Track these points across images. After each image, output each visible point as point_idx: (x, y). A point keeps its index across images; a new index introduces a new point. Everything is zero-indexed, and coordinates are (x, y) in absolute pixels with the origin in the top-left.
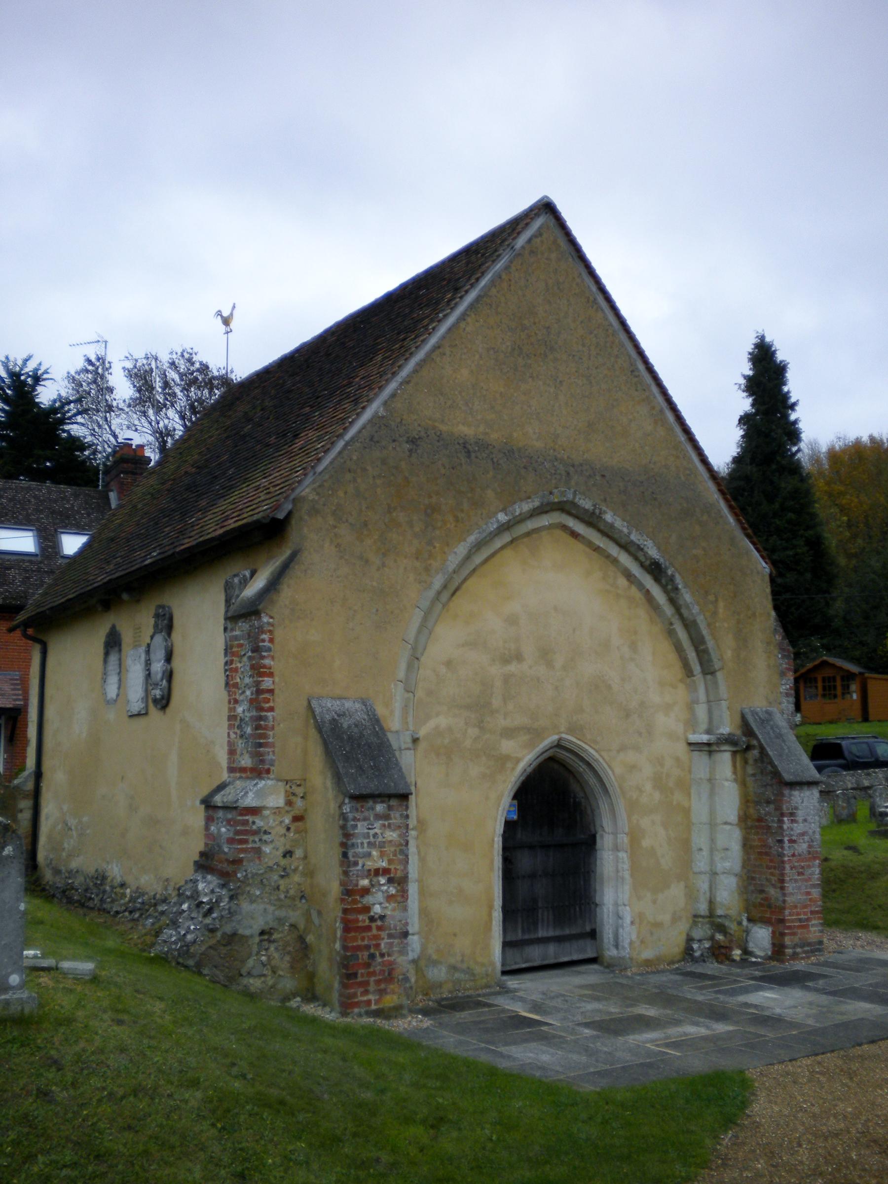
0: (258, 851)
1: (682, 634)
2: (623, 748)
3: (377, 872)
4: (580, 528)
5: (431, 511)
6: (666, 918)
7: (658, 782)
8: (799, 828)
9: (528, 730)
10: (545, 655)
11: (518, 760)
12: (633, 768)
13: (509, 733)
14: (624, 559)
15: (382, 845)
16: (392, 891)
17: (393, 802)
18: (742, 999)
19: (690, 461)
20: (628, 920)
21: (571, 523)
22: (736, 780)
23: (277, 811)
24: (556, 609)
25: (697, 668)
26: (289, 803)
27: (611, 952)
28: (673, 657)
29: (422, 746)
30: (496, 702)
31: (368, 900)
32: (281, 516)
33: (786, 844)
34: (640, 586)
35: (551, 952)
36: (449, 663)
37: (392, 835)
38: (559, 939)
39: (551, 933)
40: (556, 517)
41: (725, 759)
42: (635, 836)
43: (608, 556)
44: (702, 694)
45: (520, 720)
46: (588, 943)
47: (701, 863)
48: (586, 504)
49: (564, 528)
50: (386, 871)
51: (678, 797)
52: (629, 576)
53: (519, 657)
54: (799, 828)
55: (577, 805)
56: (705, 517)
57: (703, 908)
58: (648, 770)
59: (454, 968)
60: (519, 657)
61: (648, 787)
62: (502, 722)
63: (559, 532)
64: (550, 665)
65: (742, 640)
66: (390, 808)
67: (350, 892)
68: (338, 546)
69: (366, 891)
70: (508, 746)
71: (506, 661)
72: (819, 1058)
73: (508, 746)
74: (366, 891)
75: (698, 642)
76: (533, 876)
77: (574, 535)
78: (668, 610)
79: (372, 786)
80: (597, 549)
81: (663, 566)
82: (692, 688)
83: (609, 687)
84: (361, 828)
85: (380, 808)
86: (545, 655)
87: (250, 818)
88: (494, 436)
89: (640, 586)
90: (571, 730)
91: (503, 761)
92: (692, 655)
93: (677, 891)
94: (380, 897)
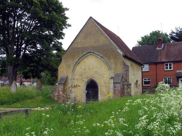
2: (99, 79)
7: (104, 83)
9: (87, 77)
10: (89, 69)
12: (100, 81)
13: (84, 78)
40: (90, 53)
48: (92, 51)
51: (107, 85)
52: (101, 59)
53: (86, 69)
58: (103, 82)
60: (86, 69)
61: (103, 83)
64: (90, 70)
65: (115, 64)
69: (60, 92)
70: (84, 79)
72: (172, 130)
73: (84, 79)
74: (60, 92)
80: (82, 60)
81: (136, 46)
83: (97, 72)
86: (89, 69)
90: (92, 77)
91: (83, 81)
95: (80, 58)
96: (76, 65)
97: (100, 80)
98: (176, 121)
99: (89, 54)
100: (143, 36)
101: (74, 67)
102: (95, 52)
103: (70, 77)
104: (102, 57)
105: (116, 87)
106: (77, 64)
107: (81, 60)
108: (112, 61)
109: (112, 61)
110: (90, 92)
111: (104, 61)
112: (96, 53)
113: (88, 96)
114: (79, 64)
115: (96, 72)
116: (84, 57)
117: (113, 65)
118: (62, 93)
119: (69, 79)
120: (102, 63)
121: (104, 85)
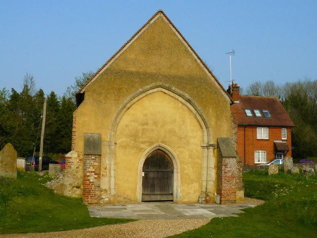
0: (70, 166)
1: (199, 118)
2: (179, 147)
3: (92, 172)
4: (167, 91)
5: (119, 89)
6: (192, 192)
7: (190, 157)
8: (227, 169)
9: (149, 142)
11: (146, 149)
13: (143, 143)
14: (180, 99)
15: (93, 166)
16: (96, 176)
17: (97, 156)
18: (163, 213)
19: (205, 72)
20: (179, 191)
21: (164, 90)
22: (214, 157)
23: (75, 158)
24: (159, 112)
25: (204, 127)
26: (78, 156)
27: (175, 199)
28: (197, 124)
29: (117, 145)
30: (140, 135)
31: (89, 178)
32: (82, 92)
33: (223, 173)
34: (186, 106)
35: (159, 198)
36: (127, 126)
37: (97, 164)
38: (161, 195)
39: (159, 193)
41: (211, 149)
42: (183, 169)
43: (175, 98)
44: (206, 134)
45: (147, 139)
46: (170, 196)
47: (204, 178)
48: (167, 85)
49: (162, 92)
50: (94, 172)
52: (183, 104)
53: (147, 124)
54: (227, 169)
55: (168, 162)
56: (207, 87)
57: (204, 190)
59: (125, 198)
60: (147, 124)
61: (187, 157)
62: (141, 140)
63: (161, 93)
64: (157, 126)
65: (218, 118)
66: (96, 158)
67: (85, 176)
68: (93, 98)
69: (88, 176)
70: (142, 146)
71: (143, 125)
73: (142, 146)
74: (88, 176)
75: (203, 120)
76: (154, 178)
77: (165, 93)
78: (195, 112)
79: (92, 152)
82: (203, 132)
84: (88, 162)
85: (93, 157)
87: (69, 159)
88: (141, 70)
89: (186, 106)
91: (141, 150)
92: (202, 123)
93: (196, 186)
94: (92, 178)
95: (134, 97)
96: (123, 112)
97: (182, 149)
98: (14, 196)
99: (155, 90)
100: (85, 72)
101: (118, 114)
102: (173, 88)
103: (106, 137)
104: (189, 101)
105: (229, 166)
106: (125, 109)
107: (135, 100)
108: (211, 111)
109: (211, 111)
110: (151, 175)
111: (192, 109)
112: (177, 90)
113: (147, 183)
114: (129, 108)
115: (172, 132)
116: (144, 95)
117: (214, 119)
118: (95, 178)
119: (104, 143)
120: (187, 113)
121: (190, 160)
